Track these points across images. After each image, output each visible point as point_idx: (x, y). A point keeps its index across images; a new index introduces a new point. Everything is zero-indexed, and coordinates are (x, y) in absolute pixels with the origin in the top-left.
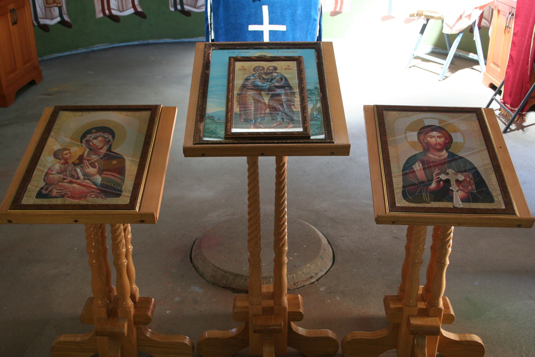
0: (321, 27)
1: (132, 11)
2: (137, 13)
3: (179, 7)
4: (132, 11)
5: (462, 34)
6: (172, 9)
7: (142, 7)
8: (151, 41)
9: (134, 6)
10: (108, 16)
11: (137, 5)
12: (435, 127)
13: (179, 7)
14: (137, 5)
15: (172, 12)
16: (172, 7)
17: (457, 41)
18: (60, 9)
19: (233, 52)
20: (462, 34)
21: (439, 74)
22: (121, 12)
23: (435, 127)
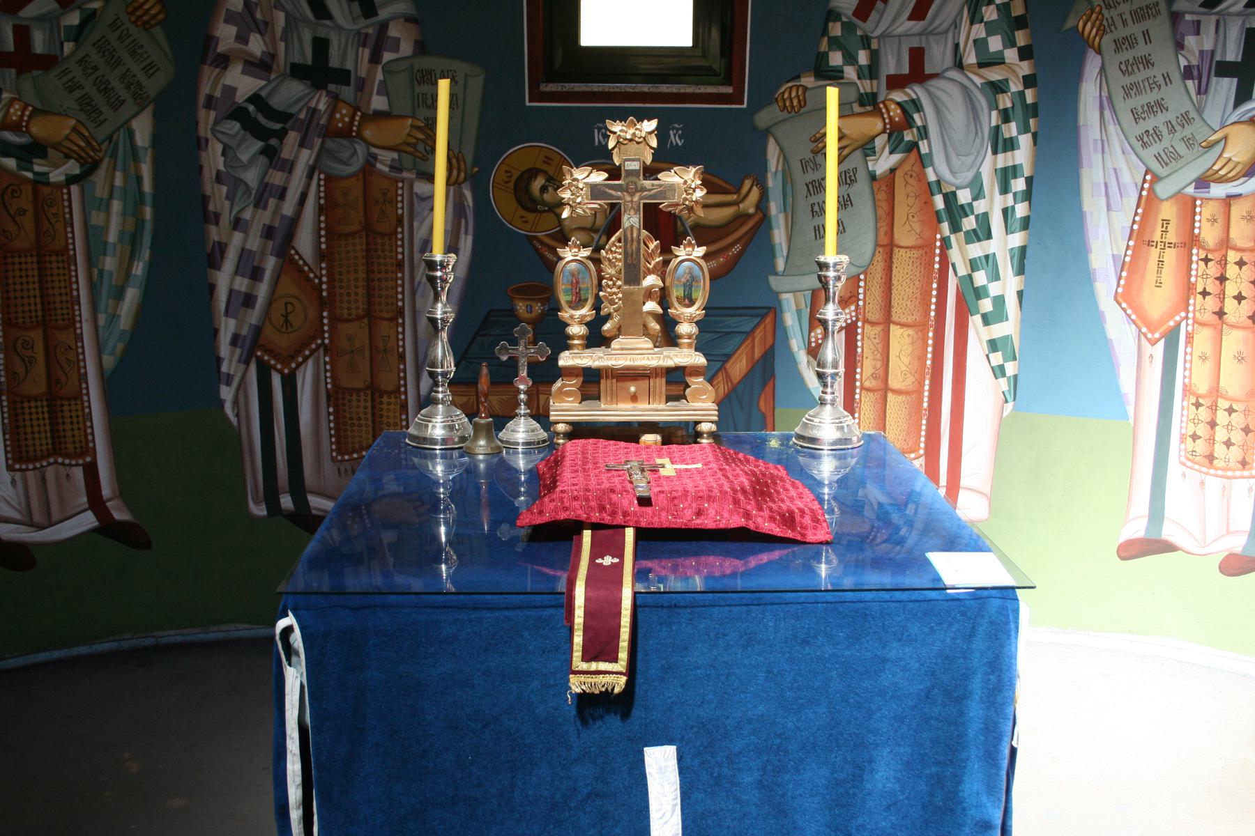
0: (707, 544)
1: (88, 520)
2: (107, 527)
3: (286, 502)
4: (88, 520)
5: (1163, 339)
6: (259, 510)
7: (130, 506)
8: (171, 636)
9: (96, 503)
10: (290, 516)
11: (110, 500)
12: (218, 256)
13: (286, 502)
14: (110, 500)
15: (259, 519)
16: (256, 502)
17: (661, 770)
18: (91, 473)
19: (657, 87)
20: (1163, 339)
21: (1017, 398)
22: (41, 527)
23: (218, 256)
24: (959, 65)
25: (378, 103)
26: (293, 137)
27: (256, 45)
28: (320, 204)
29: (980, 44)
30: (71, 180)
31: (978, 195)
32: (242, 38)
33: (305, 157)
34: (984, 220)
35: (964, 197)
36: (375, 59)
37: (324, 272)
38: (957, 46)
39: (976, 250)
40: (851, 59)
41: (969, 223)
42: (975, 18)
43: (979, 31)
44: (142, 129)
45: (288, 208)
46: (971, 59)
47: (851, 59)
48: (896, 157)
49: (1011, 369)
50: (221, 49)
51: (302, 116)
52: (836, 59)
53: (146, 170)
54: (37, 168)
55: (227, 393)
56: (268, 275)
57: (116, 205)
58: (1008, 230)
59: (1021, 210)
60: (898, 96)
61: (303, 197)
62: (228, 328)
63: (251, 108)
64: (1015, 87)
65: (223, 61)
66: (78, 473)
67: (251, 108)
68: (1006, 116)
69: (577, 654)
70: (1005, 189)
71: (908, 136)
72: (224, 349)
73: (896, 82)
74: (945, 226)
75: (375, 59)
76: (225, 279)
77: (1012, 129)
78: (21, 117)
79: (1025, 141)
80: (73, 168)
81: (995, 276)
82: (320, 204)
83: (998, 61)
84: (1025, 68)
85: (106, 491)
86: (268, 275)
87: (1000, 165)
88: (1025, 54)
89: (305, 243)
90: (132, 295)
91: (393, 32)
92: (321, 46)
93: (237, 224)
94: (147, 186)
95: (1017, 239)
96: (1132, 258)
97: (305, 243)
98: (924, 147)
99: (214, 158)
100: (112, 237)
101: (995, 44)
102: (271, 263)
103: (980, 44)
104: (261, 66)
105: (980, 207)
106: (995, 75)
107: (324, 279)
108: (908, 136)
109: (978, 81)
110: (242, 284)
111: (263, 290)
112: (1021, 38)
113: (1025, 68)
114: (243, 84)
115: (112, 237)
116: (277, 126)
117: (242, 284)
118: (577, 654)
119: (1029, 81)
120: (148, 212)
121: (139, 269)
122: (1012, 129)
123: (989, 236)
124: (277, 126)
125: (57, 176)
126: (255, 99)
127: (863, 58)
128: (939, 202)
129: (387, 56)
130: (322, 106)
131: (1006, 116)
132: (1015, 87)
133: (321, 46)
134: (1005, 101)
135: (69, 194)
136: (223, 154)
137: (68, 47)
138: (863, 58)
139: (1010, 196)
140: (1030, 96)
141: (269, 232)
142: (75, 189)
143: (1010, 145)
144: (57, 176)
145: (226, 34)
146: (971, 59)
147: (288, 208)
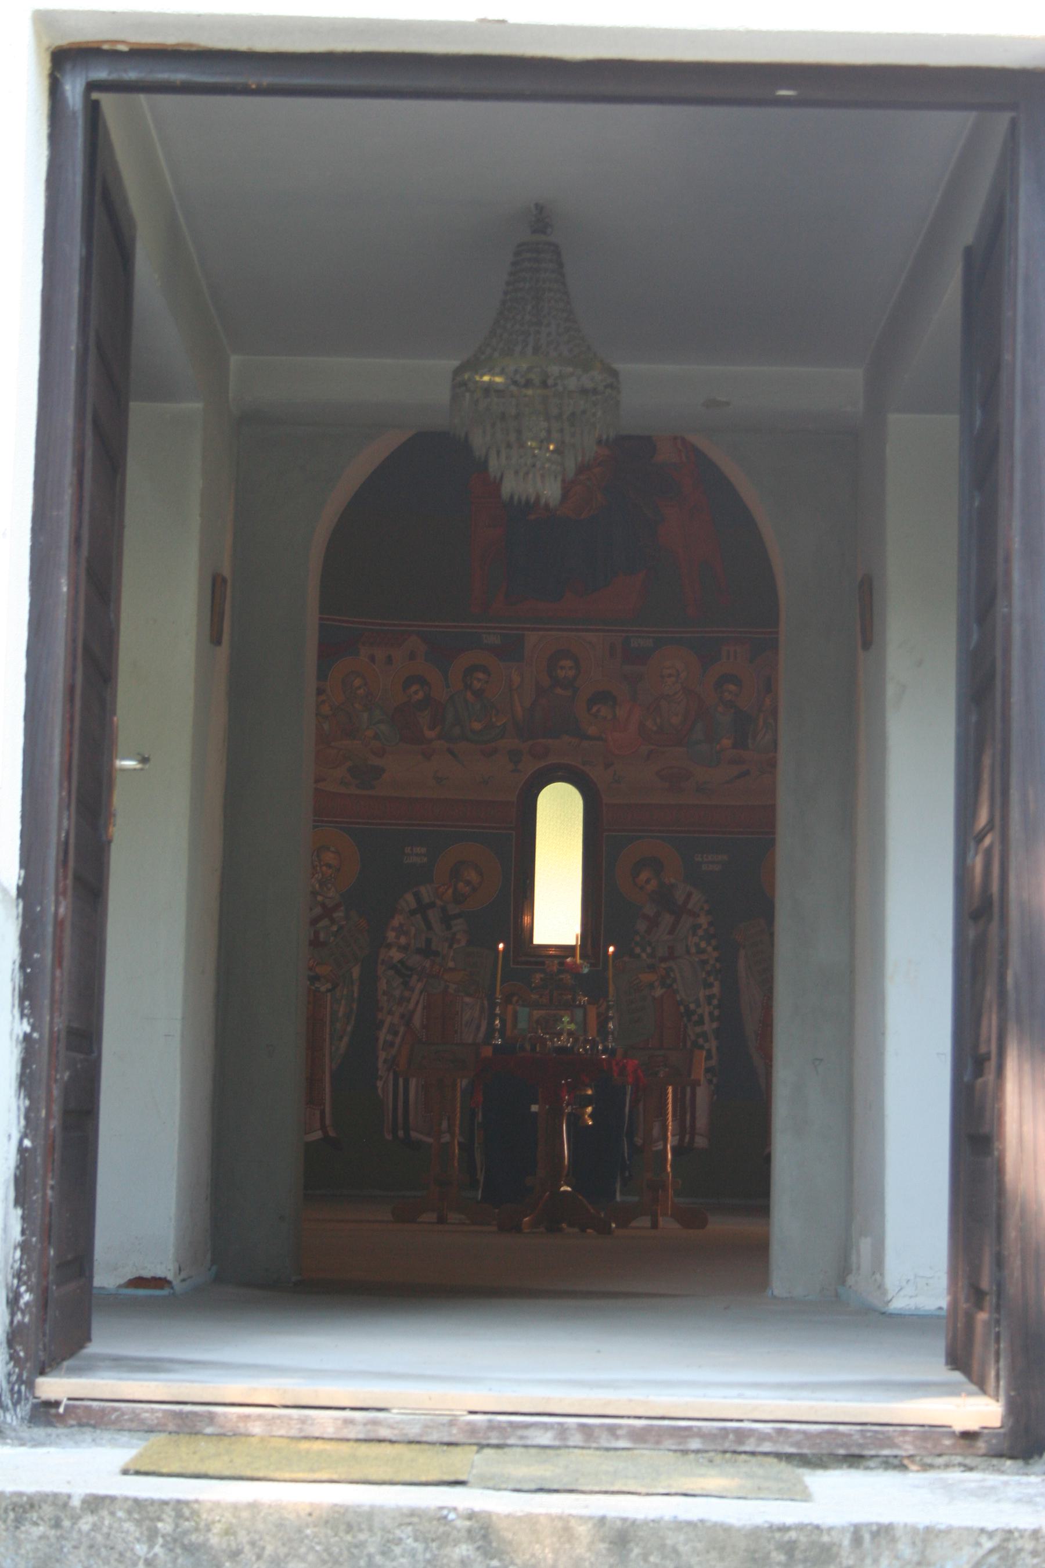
1: (318, 1135)
3: (401, 1133)
9: (323, 1128)
13: (401, 1133)
18: (323, 1112)
24: (688, 952)
25: (451, 964)
26: (415, 978)
27: (403, 940)
28: (41, 904)
29: (697, 945)
30: (328, 991)
31: (698, 1006)
32: (398, 937)
33: (419, 986)
34: (701, 1016)
35: (692, 1006)
36: (450, 947)
37: (424, 1034)
38: (687, 946)
39: (698, 1029)
40: (644, 950)
41: (695, 1018)
42: (694, 934)
43: (696, 939)
44: (356, 972)
45: (411, 1006)
46: (693, 950)
47: (644, 950)
48: (664, 990)
49: (715, 1080)
50: (389, 941)
51: (419, 969)
52: (638, 950)
53: (356, 989)
54: (316, 985)
55: (380, 1084)
56: (401, 1034)
57: (343, 1002)
58: (712, 1021)
59: (716, 1013)
60: (663, 965)
61: (418, 1002)
62: (382, 1055)
63: (399, 965)
64: (712, 962)
65: (389, 946)
66: (318, 1113)
67: (399, 965)
68: (708, 973)
69: (511, 964)
70: (709, 1004)
71: (668, 982)
72: (380, 1065)
73: (663, 960)
74: (685, 1019)
75: (450, 947)
76: (383, 1035)
77: (711, 979)
78: (313, 965)
79: (717, 984)
80: (329, 986)
81: (707, 1040)
82: (41, 904)
83: (703, 951)
84: (716, 954)
85: (328, 1122)
86: (401, 1034)
87: (707, 994)
88: (715, 949)
89: (417, 1021)
90: (346, 1039)
91: (458, 937)
92: (428, 941)
93: (390, 1012)
94: (356, 995)
95: (715, 1025)
96: (31, 1009)
97: (417, 1021)
98: (675, 986)
99: (383, 985)
100: (341, 1014)
101: (703, 945)
102: (402, 1029)
103: (697, 945)
104: (404, 949)
105: (700, 1011)
106: (704, 957)
107: (424, 1037)
108: (668, 982)
109: (697, 959)
110: (389, 1038)
111: (398, 1040)
112: (714, 942)
113: (716, 954)
114: (396, 955)
115: (341, 1014)
116: (409, 973)
117: (389, 1038)
118: (511, 964)
119: (717, 960)
120: (355, 1006)
121: (349, 1028)
122: (711, 979)
123: (703, 1023)
124: (409, 973)
125: (323, 989)
126: (401, 961)
127: (649, 950)
128: (682, 1009)
129: (455, 946)
130: (428, 965)
131: (708, 973)
132: (712, 962)
133: (428, 941)
134: (708, 968)
135: (327, 996)
136: (387, 983)
137: (332, 938)
138: (649, 950)
139: (712, 1007)
140: (718, 965)
141: (402, 1016)
142: (329, 994)
143: (711, 985)
144: (323, 989)
145: (391, 935)
146: (693, 950)
147: (411, 1006)
